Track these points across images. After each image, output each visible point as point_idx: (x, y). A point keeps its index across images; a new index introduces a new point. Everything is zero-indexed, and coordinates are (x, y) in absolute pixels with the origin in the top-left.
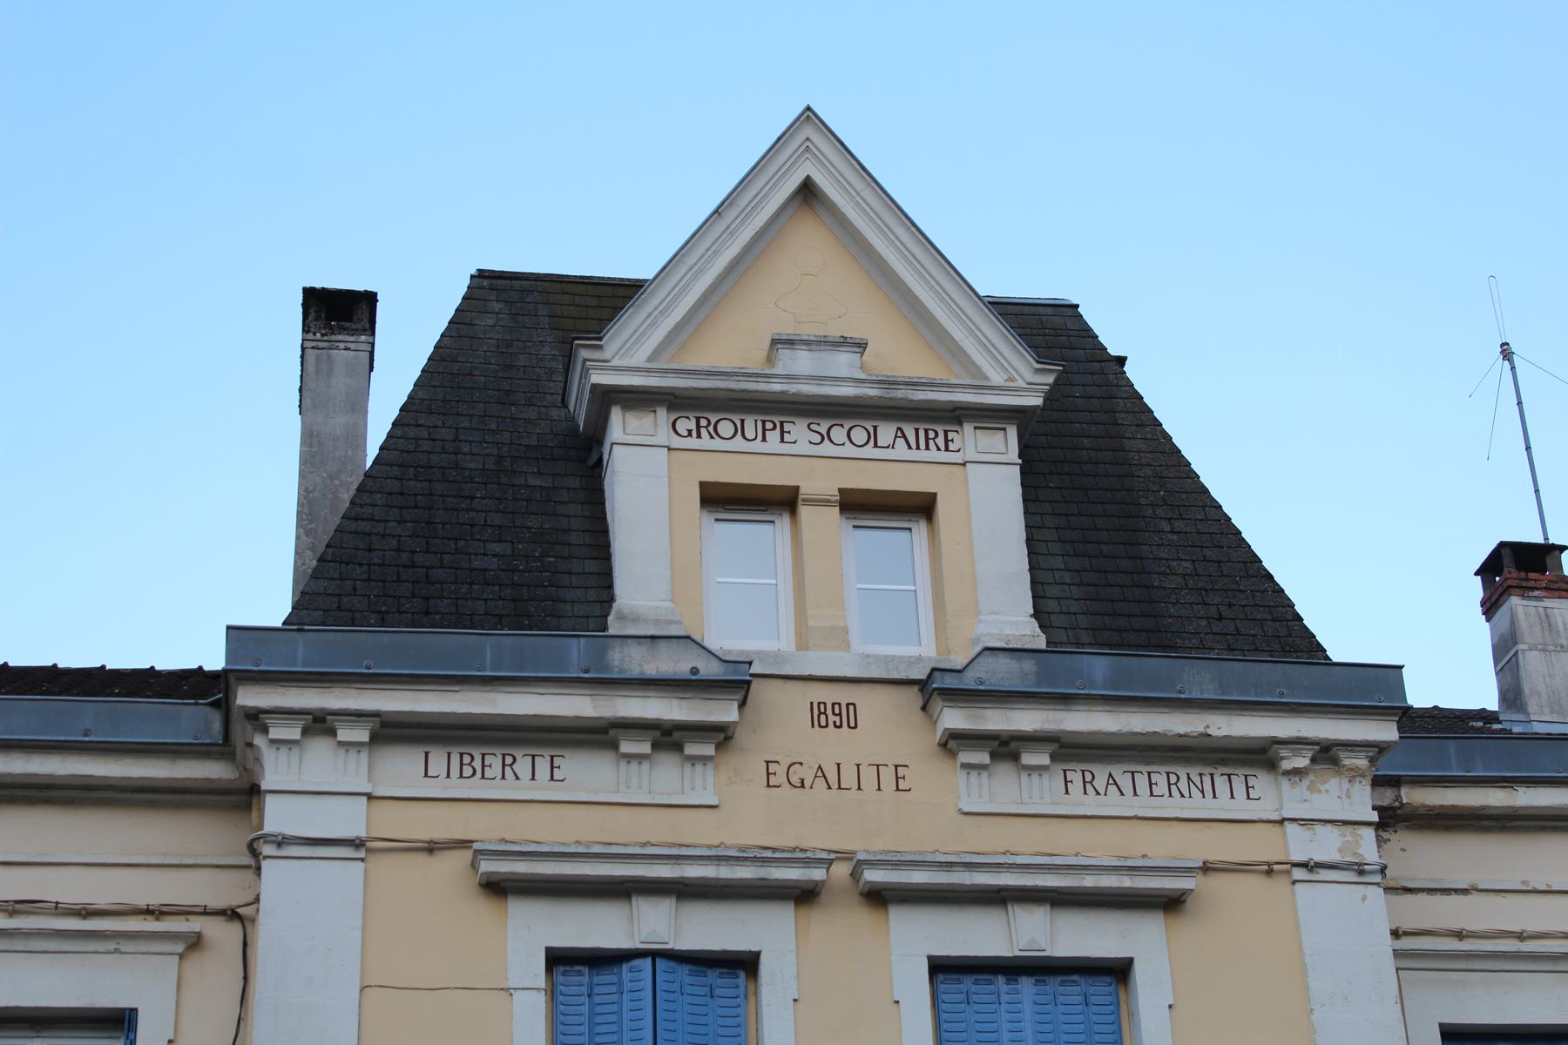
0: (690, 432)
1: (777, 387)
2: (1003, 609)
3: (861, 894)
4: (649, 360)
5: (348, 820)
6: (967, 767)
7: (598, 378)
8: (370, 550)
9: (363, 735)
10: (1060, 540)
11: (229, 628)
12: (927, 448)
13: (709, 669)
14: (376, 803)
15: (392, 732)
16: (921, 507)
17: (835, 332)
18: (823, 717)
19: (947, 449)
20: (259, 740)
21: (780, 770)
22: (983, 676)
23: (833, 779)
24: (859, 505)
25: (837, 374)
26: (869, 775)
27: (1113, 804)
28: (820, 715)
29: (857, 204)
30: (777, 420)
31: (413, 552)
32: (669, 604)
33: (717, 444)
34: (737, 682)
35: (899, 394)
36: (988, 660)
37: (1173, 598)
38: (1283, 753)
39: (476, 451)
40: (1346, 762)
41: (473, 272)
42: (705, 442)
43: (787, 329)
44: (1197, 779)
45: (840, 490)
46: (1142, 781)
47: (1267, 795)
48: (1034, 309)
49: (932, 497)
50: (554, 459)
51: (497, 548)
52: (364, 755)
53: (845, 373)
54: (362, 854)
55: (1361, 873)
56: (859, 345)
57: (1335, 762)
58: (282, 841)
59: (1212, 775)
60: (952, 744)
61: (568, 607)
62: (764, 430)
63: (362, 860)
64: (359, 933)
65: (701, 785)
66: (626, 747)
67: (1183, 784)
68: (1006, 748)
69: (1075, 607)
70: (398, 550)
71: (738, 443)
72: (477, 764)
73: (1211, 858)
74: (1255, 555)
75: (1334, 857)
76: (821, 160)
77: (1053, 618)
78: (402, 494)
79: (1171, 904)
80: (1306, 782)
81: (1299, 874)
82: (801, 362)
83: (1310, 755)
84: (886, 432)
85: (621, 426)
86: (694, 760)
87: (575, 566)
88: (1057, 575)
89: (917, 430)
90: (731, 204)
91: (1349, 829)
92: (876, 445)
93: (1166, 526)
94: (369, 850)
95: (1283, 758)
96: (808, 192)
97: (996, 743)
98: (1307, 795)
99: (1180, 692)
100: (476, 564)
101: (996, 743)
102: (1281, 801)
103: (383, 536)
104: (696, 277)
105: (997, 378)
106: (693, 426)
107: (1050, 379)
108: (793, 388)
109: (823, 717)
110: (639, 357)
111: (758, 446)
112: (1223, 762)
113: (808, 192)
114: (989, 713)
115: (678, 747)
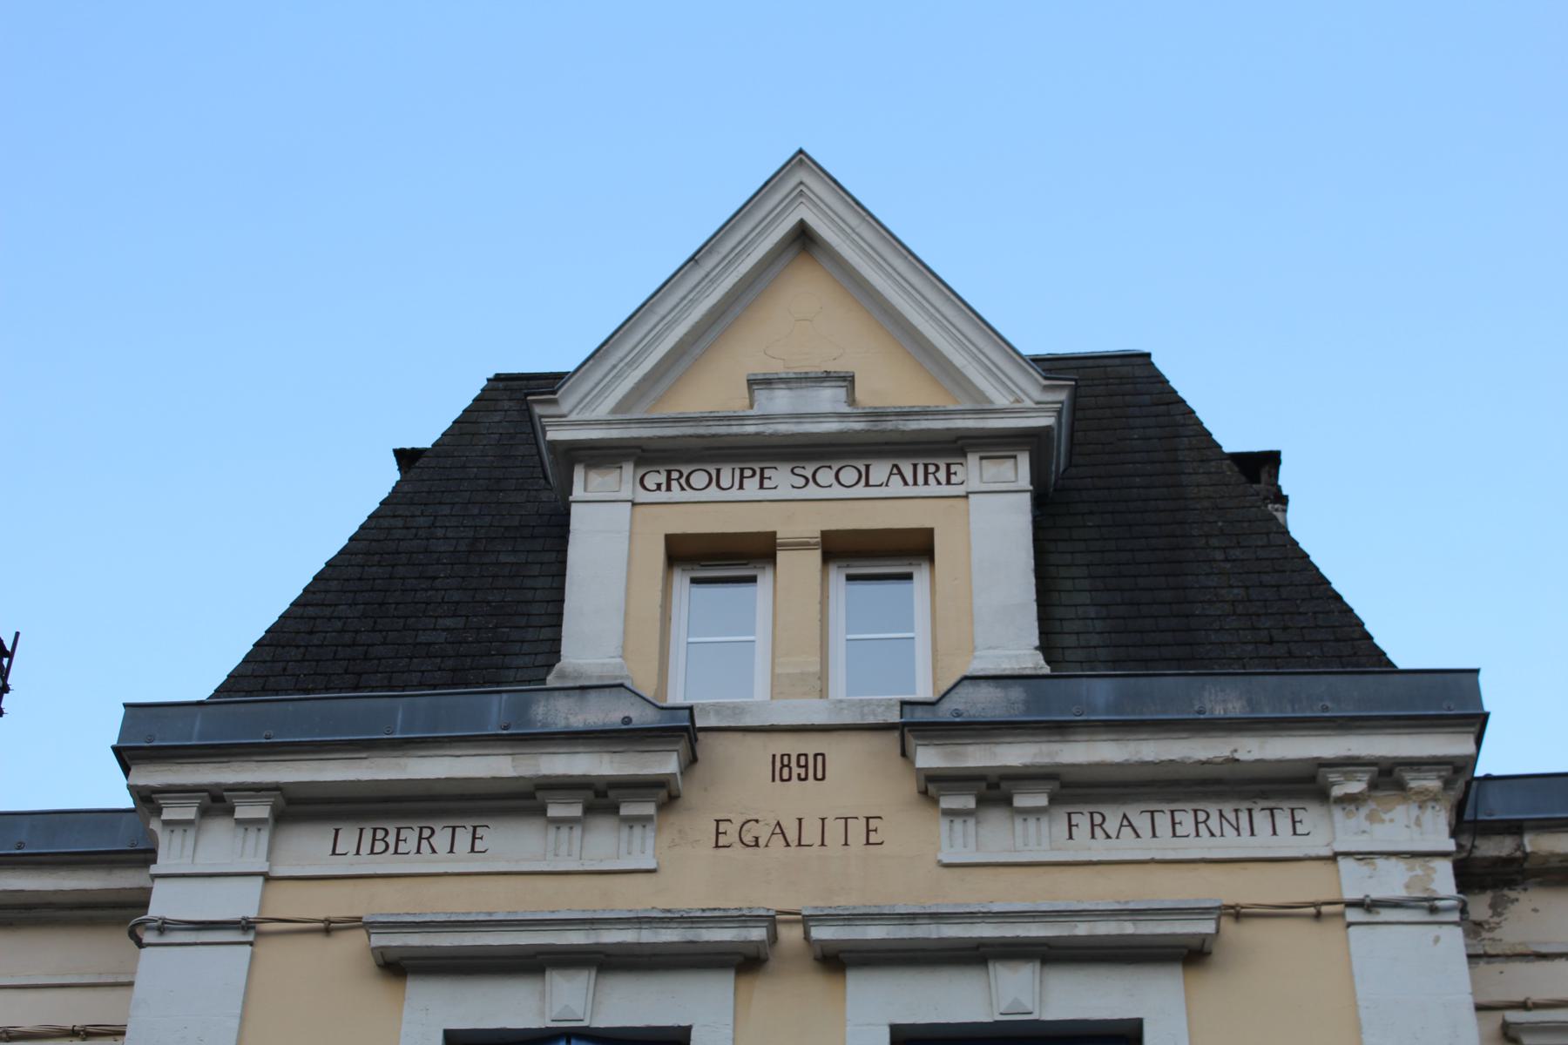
0: (659, 486)
1: (751, 429)
2: (1014, 645)
3: (816, 959)
4: (614, 411)
5: (241, 901)
6: (951, 813)
7: (553, 435)
8: (311, 633)
9: (263, 811)
10: (1090, 577)
11: (125, 705)
12: (926, 483)
13: (643, 717)
14: (274, 885)
15: (296, 808)
16: (911, 549)
17: (817, 366)
18: (786, 770)
19: (949, 482)
20: (155, 825)
21: (732, 830)
22: (960, 707)
23: (792, 835)
24: (845, 550)
25: (822, 410)
26: (835, 830)
27: (1127, 847)
28: (782, 769)
29: (853, 241)
30: (757, 467)
31: (357, 632)
32: (619, 660)
33: (689, 495)
34: (681, 731)
35: (889, 426)
36: (967, 691)
37: (1216, 625)
38: (1333, 777)
39: (450, 535)
40: (1413, 784)
41: (491, 376)
42: (676, 494)
43: (760, 368)
44: (1231, 816)
45: (823, 533)
46: (1163, 821)
47: (1319, 830)
48: (1090, 363)
49: (928, 534)
50: (533, 537)
51: (449, 622)
52: (265, 835)
53: (827, 408)
54: (250, 938)
55: (1433, 910)
56: (844, 379)
57: (1401, 786)
58: (164, 926)
59: (1250, 811)
60: (932, 789)
61: (512, 673)
62: (742, 477)
63: (251, 944)
64: (235, 1023)
65: (640, 849)
66: (554, 811)
67: (1214, 823)
68: (994, 791)
69: (1095, 640)
70: (342, 631)
71: (713, 493)
72: (391, 840)
73: (1243, 901)
74: (1322, 577)
75: (1399, 892)
76: (817, 204)
77: (1068, 652)
78: (360, 579)
79: (1191, 955)
80: (1364, 811)
81: (1353, 915)
82: (780, 401)
83: (1366, 778)
84: (880, 470)
85: (586, 485)
86: (631, 821)
87: (531, 634)
88: (1080, 610)
89: (915, 466)
90: (710, 252)
91: (1418, 862)
92: (867, 484)
93: (1219, 555)
94: (259, 934)
95: (1333, 784)
96: (798, 235)
97: (983, 785)
98: (1365, 825)
99: (1199, 712)
100: (422, 638)
101: (983, 785)
102: (1334, 833)
103: (329, 619)
104: (669, 327)
105: (1001, 400)
106: (662, 479)
107: (1063, 396)
108: (769, 429)
109: (786, 770)
110: (603, 410)
111: (735, 494)
112: (1264, 795)
113: (798, 235)
114: (971, 749)
115: (613, 810)
